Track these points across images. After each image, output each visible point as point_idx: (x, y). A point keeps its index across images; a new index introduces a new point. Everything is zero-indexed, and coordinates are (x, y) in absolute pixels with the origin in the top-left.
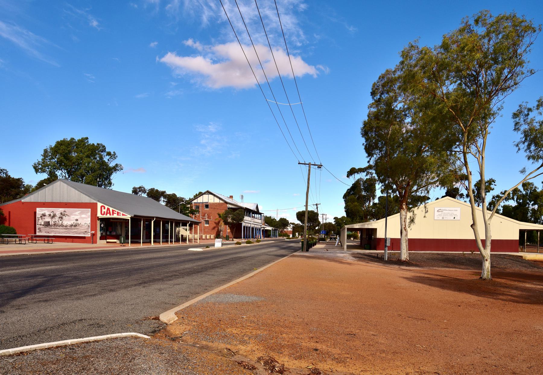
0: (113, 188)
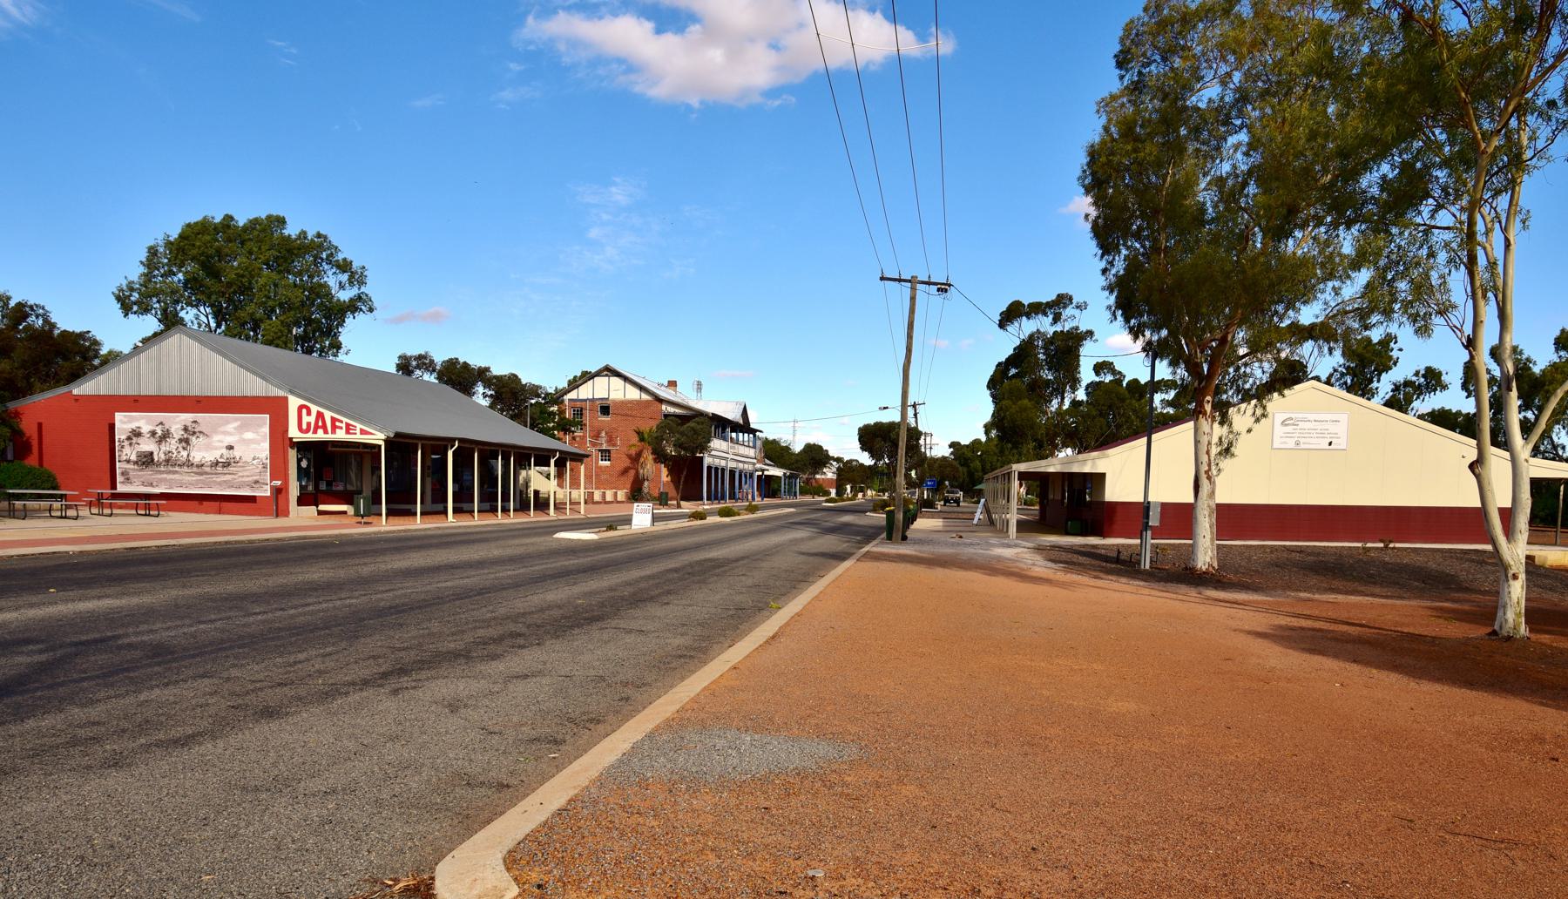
0: (342, 357)
